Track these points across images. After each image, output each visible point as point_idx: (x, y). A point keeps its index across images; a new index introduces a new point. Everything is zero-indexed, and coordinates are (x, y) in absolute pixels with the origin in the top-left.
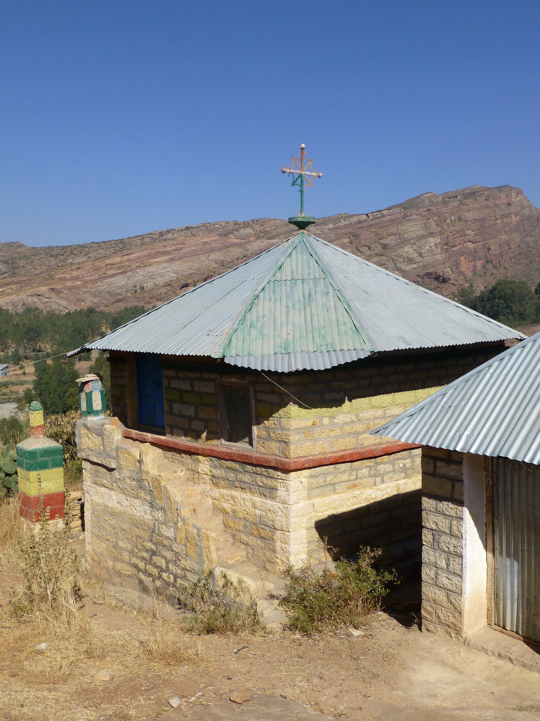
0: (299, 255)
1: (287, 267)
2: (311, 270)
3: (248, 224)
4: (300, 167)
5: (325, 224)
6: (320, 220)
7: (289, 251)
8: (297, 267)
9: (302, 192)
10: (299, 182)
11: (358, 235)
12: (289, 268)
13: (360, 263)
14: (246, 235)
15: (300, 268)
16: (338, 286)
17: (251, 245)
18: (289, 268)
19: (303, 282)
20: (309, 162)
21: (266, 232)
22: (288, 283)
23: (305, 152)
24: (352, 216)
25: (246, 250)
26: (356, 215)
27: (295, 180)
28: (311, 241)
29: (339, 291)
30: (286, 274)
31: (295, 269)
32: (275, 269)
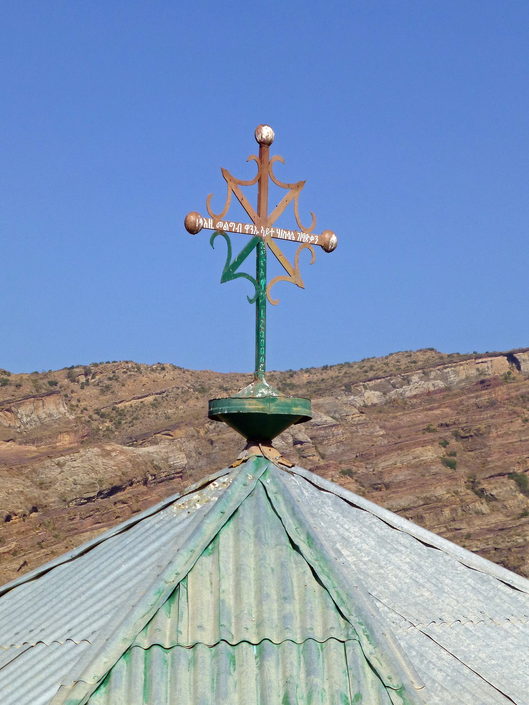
0: (249, 544)
1: (200, 594)
2: (294, 608)
3: (53, 383)
4: (253, 212)
5: (348, 389)
6: (332, 373)
7: (209, 529)
8: (238, 596)
9: (259, 302)
10: (249, 266)
11: (479, 434)
12: (208, 598)
13: (484, 582)
14: (44, 426)
15: (250, 598)
16: (399, 673)
17: (59, 464)
18: (208, 598)
19: (261, 656)
20: (290, 195)
21: (121, 413)
22: (205, 654)
23: (274, 155)
24: (455, 359)
25: (41, 485)
26: (467, 357)
27: (235, 257)
28: (295, 492)
29: (401, 691)
30: (195, 621)
31: (230, 600)
32: (152, 598)
